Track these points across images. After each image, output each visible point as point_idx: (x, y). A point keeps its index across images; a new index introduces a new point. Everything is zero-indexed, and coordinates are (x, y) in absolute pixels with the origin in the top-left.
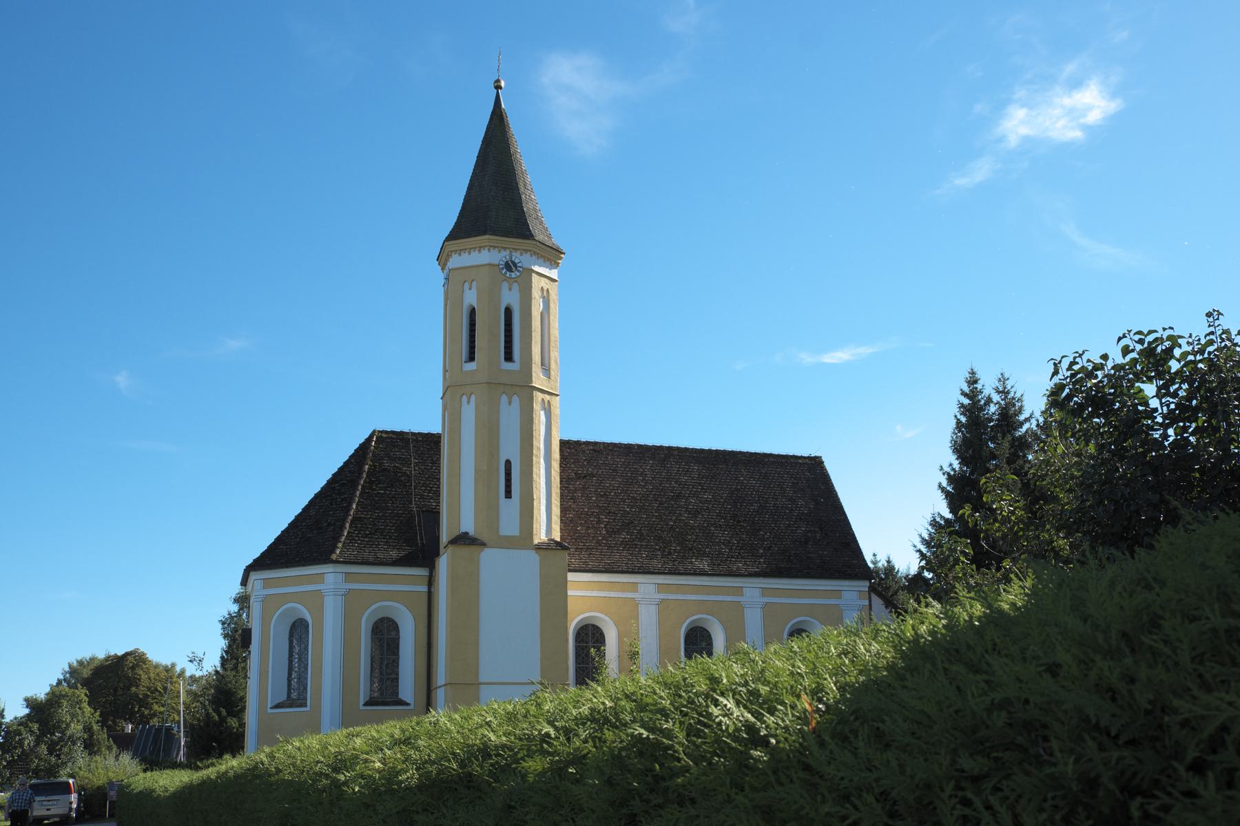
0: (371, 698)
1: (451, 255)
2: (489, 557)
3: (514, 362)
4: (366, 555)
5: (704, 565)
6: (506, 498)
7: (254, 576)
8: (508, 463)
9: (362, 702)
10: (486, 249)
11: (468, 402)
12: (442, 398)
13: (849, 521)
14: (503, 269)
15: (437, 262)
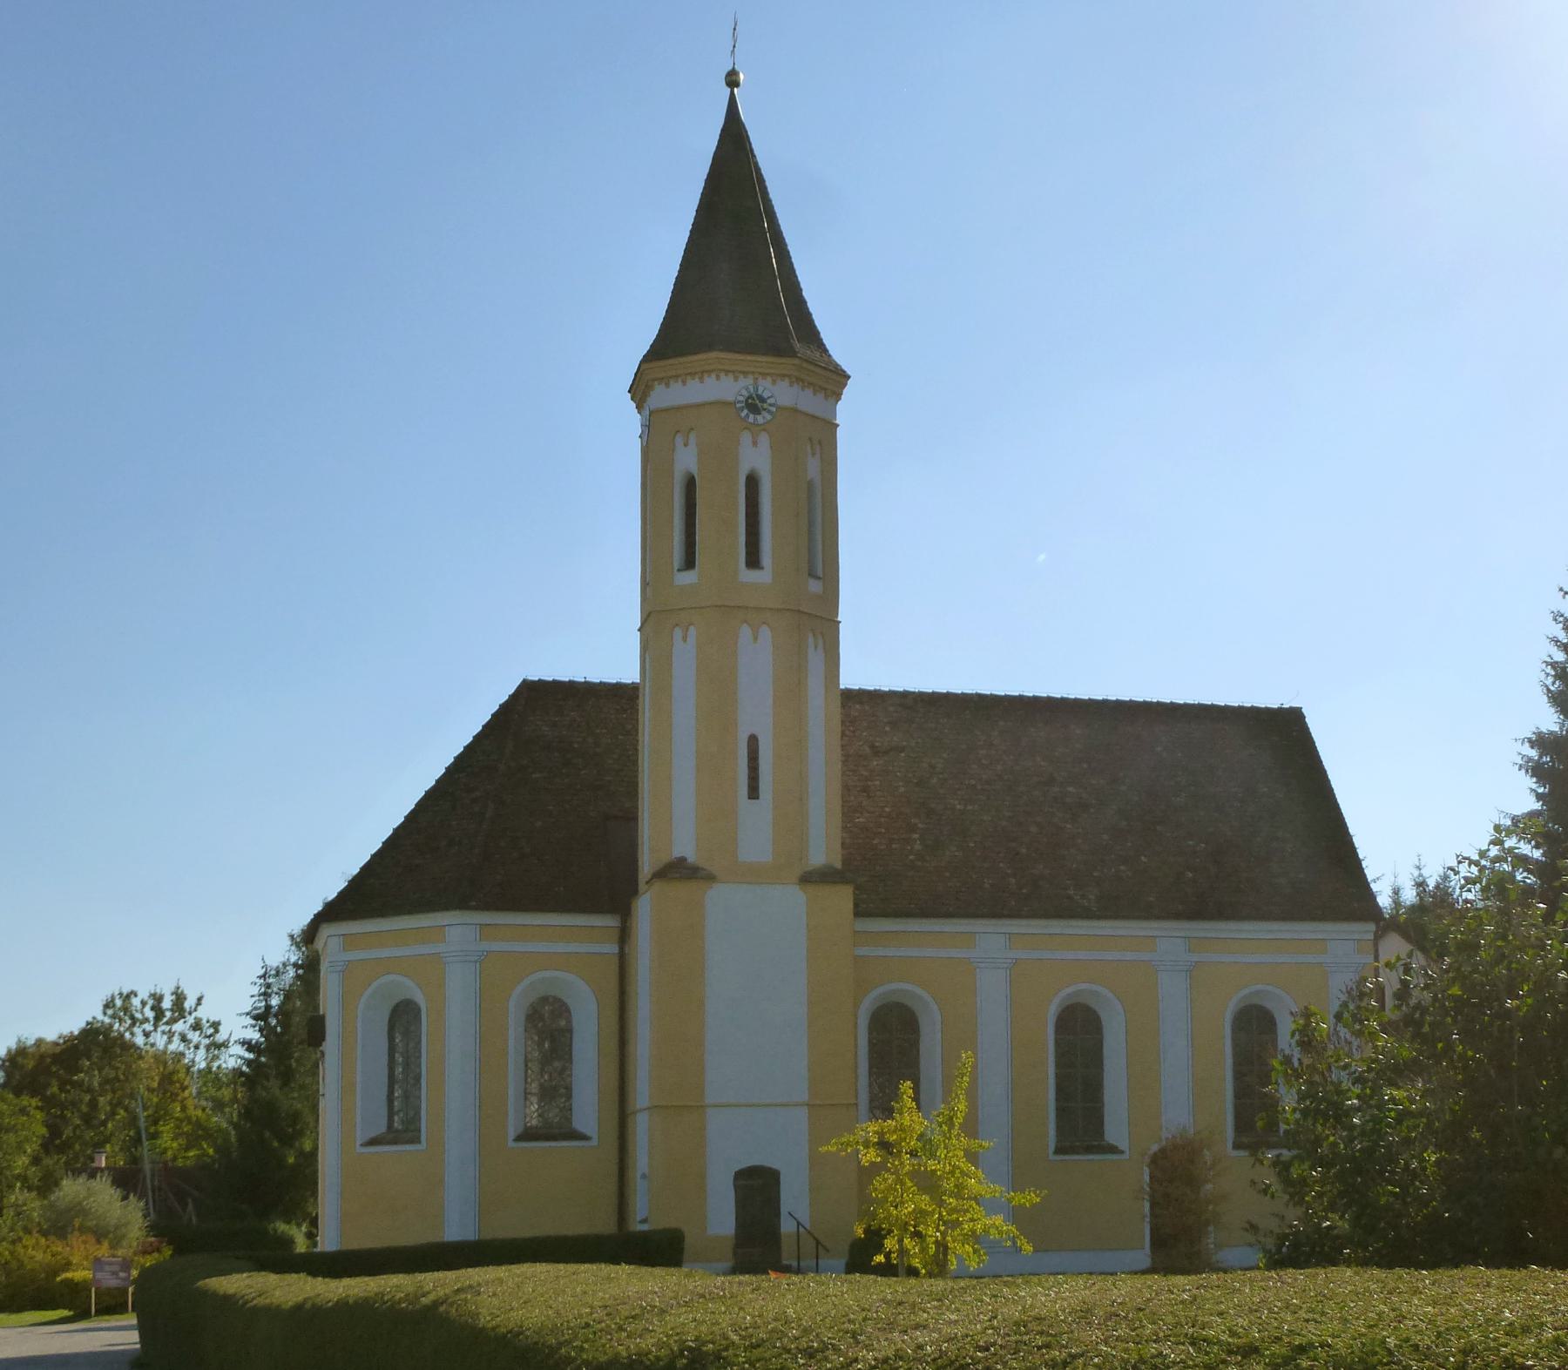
3: (762, 568)
8: (753, 741)
10: (714, 376)
11: (685, 639)
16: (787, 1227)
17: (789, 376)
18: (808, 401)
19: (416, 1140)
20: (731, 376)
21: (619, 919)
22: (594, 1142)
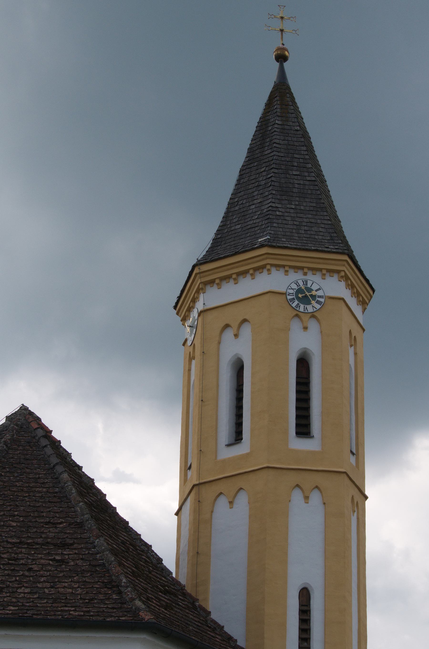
3: (313, 437)
6: (183, 345)
10: (265, 271)
12: (177, 514)
13: (367, 645)
14: (293, 300)
15: (175, 312)
20: (282, 270)
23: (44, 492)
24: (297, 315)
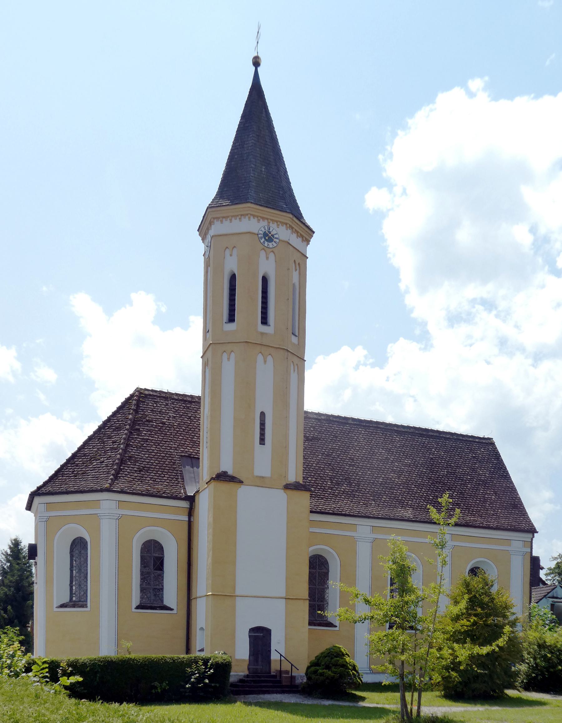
0: (140, 603)
1: (213, 222)
2: (243, 492)
3: (270, 326)
4: (139, 487)
5: (409, 513)
7: (37, 500)
8: (263, 415)
9: (134, 606)
10: (247, 217)
11: (229, 359)
16: (274, 656)
17: (286, 224)
18: (295, 241)
19: (84, 606)
21: (189, 504)
22: (175, 612)
23: (361, 681)
24: (263, 249)
